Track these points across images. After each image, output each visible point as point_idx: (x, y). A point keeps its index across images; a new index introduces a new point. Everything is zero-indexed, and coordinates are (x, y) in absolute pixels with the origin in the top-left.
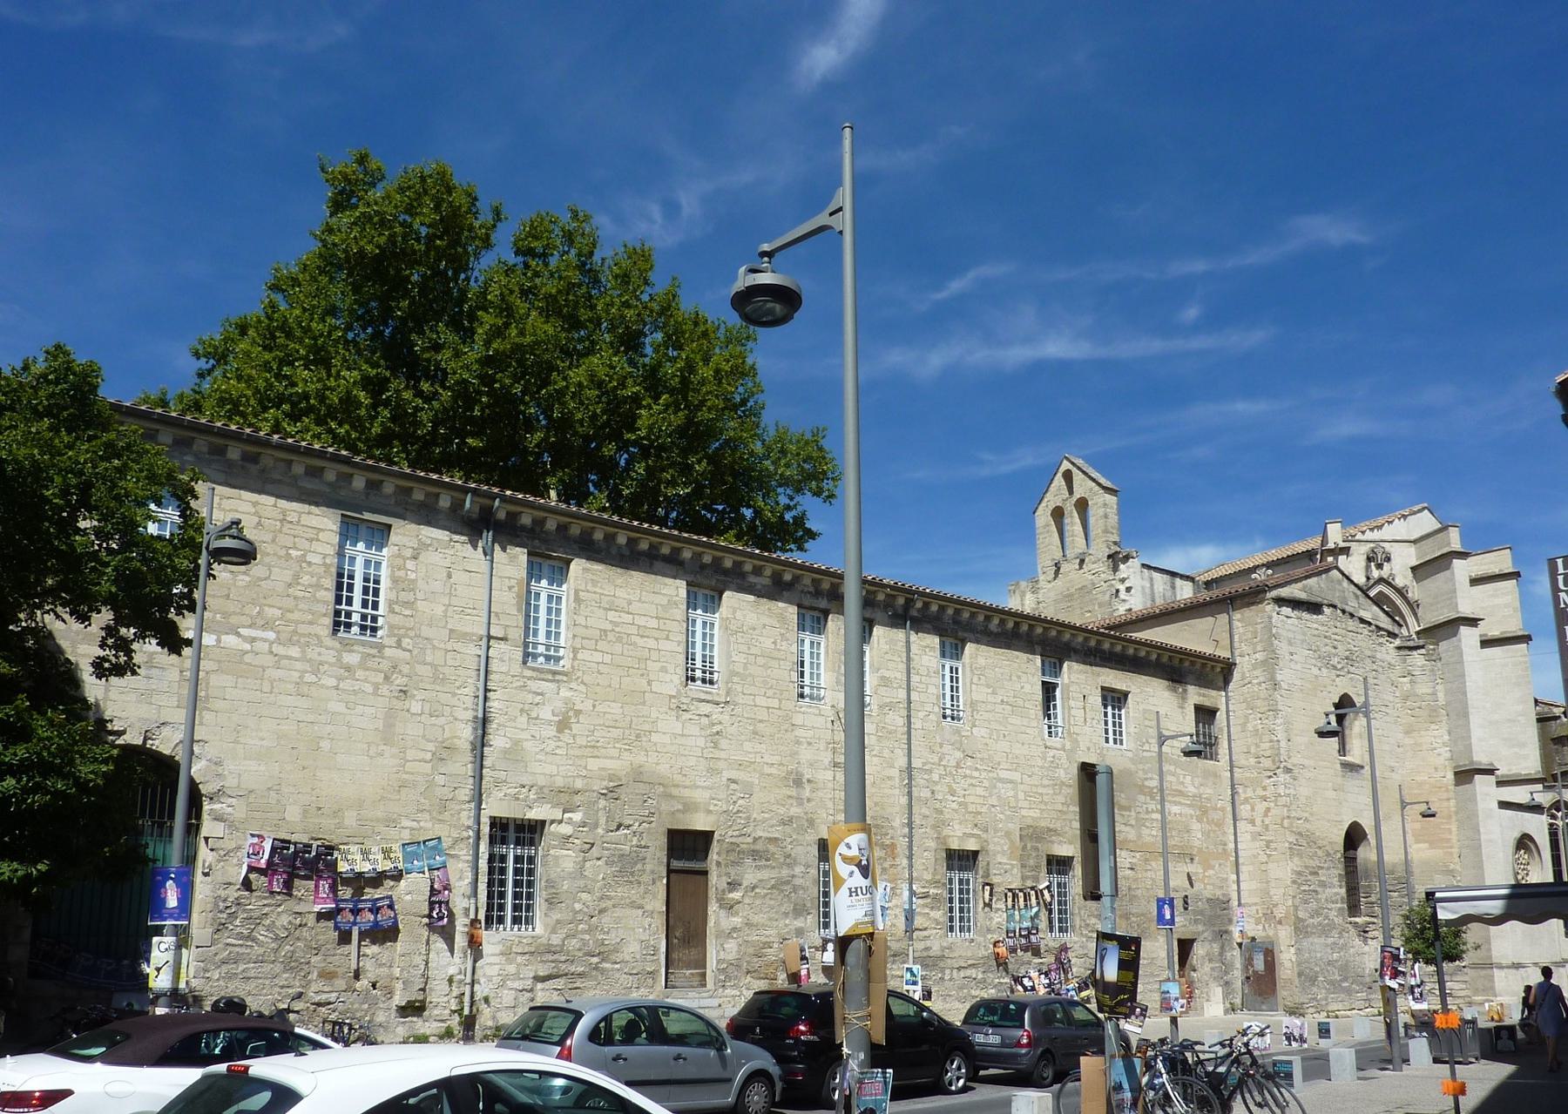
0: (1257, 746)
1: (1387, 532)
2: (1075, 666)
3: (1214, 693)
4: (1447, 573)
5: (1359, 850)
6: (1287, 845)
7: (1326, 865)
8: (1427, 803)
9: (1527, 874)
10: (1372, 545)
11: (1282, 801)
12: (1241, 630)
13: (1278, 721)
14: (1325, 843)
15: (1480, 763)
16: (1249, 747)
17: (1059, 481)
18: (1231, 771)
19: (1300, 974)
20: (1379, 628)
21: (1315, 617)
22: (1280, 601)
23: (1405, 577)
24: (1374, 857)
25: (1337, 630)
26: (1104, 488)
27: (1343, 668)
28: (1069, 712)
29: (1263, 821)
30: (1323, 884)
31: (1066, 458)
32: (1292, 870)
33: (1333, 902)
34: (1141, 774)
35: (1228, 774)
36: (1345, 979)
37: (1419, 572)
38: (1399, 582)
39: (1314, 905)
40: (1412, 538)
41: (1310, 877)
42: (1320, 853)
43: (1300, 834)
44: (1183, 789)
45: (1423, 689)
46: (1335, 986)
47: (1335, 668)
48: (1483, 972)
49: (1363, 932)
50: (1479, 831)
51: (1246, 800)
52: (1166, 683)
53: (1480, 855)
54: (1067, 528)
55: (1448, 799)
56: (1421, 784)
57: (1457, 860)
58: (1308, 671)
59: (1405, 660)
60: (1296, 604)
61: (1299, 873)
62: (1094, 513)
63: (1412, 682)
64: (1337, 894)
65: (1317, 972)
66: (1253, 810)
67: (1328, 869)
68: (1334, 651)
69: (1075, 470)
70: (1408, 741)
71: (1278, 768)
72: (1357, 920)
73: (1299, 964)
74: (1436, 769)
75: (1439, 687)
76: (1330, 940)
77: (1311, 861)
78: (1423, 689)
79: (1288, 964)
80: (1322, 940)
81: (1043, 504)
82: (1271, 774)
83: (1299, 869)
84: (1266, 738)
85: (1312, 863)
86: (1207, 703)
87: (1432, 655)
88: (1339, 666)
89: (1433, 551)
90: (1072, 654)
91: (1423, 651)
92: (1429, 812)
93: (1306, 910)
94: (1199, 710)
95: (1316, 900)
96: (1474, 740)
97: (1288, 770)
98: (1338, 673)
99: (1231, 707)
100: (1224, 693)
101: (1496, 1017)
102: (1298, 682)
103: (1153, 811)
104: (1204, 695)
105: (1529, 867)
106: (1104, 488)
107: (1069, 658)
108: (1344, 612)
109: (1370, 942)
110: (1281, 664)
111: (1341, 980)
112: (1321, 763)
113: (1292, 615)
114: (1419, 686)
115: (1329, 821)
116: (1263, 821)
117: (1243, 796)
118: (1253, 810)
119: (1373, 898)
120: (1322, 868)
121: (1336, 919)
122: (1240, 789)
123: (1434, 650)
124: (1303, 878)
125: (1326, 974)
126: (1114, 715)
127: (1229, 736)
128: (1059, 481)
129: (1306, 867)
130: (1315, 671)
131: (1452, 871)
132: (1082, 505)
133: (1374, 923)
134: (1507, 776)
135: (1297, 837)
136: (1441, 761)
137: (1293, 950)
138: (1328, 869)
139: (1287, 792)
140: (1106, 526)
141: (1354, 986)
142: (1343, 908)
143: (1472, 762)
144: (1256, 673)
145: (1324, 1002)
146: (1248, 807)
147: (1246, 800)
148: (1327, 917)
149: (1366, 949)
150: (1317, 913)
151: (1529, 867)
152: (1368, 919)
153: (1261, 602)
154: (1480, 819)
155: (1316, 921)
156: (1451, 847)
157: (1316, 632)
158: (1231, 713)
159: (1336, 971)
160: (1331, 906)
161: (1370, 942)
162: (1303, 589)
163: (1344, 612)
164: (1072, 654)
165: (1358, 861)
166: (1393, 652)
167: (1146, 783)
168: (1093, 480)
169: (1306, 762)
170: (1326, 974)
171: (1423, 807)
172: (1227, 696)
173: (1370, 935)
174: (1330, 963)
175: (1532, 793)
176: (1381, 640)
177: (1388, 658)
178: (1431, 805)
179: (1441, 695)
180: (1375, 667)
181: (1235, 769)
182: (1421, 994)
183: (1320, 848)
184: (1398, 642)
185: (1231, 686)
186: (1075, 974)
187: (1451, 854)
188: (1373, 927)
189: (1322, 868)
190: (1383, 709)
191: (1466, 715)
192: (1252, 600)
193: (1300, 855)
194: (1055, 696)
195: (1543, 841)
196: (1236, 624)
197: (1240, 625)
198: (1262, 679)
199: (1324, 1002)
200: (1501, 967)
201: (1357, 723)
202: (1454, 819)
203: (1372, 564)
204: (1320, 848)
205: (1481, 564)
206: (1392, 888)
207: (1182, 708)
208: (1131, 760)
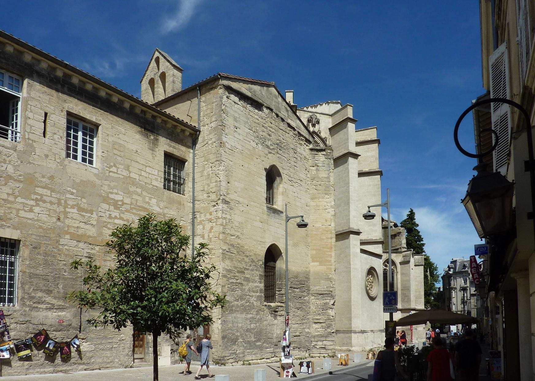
0: (209, 185)
1: (319, 109)
2: (37, 86)
3: (183, 148)
4: (345, 130)
5: (277, 262)
6: (221, 251)
7: (250, 268)
8: (302, 217)
9: (372, 287)
10: (311, 114)
11: (220, 221)
12: (205, 108)
13: (222, 168)
14: (251, 254)
15: (353, 229)
16: (204, 187)
17: (153, 63)
18: (193, 203)
19: (223, 338)
20: (300, 135)
21: (256, 111)
22: (229, 89)
23: (326, 133)
24: (284, 267)
25: (272, 125)
26: (173, 65)
27: (273, 149)
28: (26, 123)
29: (209, 236)
30: (247, 280)
31: (157, 50)
32: (224, 268)
33: (254, 292)
34: (106, 188)
35: (191, 205)
36: (259, 340)
37: (333, 131)
38: (323, 135)
39: (239, 293)
40: (331, 113)
41: (237, 274)
42: (246, 259)
43: (232, 245)
44: (148, 207)
45: (323, 174)
46: (251, 345)
47: (268, 147)
48: (347, 335)
49: (274, 312)
50: (350, 263)
51: (201, 223)
52: (139, 129)
53: (350, 276)
54: (156, 90)
55: (331, 238)
56: (318, 229)
57: (333, 272)
58: (248, 143)
59: (314, 157)
60: (242, 97)
61: (229, 271)
62: (169, 80)
63: (317, 170)
64: (258, 287)
65: (237, 336)
66: (204, 228)
67: (252, 270)
68: (268, 137)
69: (161, 57)
70: (312, 204)
71: (219, 199)
72: (273, 305)
73: (223, 331)
74: (326, 220)
75: (331, 174)
76: (249, 316)
77: (239, 264)
78: (323, 174)
79: (216, 331)
80: (244, 316)
81: (145, 78)
82: (215, 204)
83: (230, 268)
84: (213, 180)
85: (240, 265)
86: (176, 153)
87: (329, 155)
88: (271, 147)
89: (339, 118)
90: (35, 75)
91: (324, 153)
92: (303, 223)
93: (233, 295)
94: (168, 156)
95: (241, 290)
96: (351, 217)
97: (226, 202)
98: (270, 151)
99: (196, 161)
100: (192, 151)
101: (344, 363)
102: (240, 147)
103: (116, 218)
104: (174, 147)
105: (373, 284)
106: (173, 65)
107: (31, 77)
108: (277, 116)
109: (278, 318)
110: (227, 131)
111: (255, 341)
112: (252, 203)
113: (239, 103)
114: (320, 172)
115: (255, 240)
116: (209, 236)
117: (199, 219)
118: (204, 228)
119: (283, 292)
120: (248, 269)
121: (255, 303)
122: (198, 215)
123: (330, 153)
124: (232, 274)
125: (245, 337)
126: (84, 141)
127: (194, 179)
128: (153, 63)
129: (235, 267)
130: (254, 144)
131: (330, 279)
132: (163, 76)
133: (282, 307)
134: (367, 240)
135: (230, 247)
136: (329, 216)
137: (220, 321)
138: (252, 270)
139: (224, 216)
140: (173, 87)
141: (265, 344)
142: (261, 296)
143: (349, 228)
144: (211, 136)
145: (241, 355)
146: (201, 227)
147: (201, 223)
148: (248, 301)
149: (276, 322)
150: (241, 298)
151: (373, 284)
152: (279, 304)
153: (215, 88)
154: (351, 257)
155: (240, 303)
156: (331, 265)
157: (257, 121)
158: (196, 165)
159: (253, 336)
160: (252, 294)
161: (278, 318)
162: (250, 90)
163: (277, 116)
164: (35, 75)
165: (276, 269)
166: (308, 152)
167: (111, 196)
168: (168, 61)
169: (241, 200)
170: (245, 337)
171: (298, 220)
172: (194, 152)
173: (279, 313)
174: (248, 330)
175: (369, 207)
176: (301, 142)
177: (305, 154)
178: (304, 219)
179: (332, 179)
180: (296, 156)
181: (196, 202)
182: (289, 353)
183: (247, 256)
184: (311, 146)
185: (198, 146)
186: (12, 337)
187: (331, 269)
188: (282, 309)
189: (248, 269)
190: (299, 181)
191: (348, 204)
192: (211, 87)
193: (231, 259)
194: (17, 109)
195: (380, 271)
196: (203, 104)
197: (204, 105)
198: (214, 140)
199: (241, 355)
200: (355, 332)
201: (281, 186)
202: (333, 249)
203: (310, 124)
204: (247, 256)
205: (363, 136)
206: (295, 286)
207: (153, 150)
208: (95, 175)
